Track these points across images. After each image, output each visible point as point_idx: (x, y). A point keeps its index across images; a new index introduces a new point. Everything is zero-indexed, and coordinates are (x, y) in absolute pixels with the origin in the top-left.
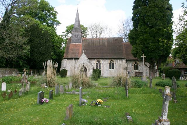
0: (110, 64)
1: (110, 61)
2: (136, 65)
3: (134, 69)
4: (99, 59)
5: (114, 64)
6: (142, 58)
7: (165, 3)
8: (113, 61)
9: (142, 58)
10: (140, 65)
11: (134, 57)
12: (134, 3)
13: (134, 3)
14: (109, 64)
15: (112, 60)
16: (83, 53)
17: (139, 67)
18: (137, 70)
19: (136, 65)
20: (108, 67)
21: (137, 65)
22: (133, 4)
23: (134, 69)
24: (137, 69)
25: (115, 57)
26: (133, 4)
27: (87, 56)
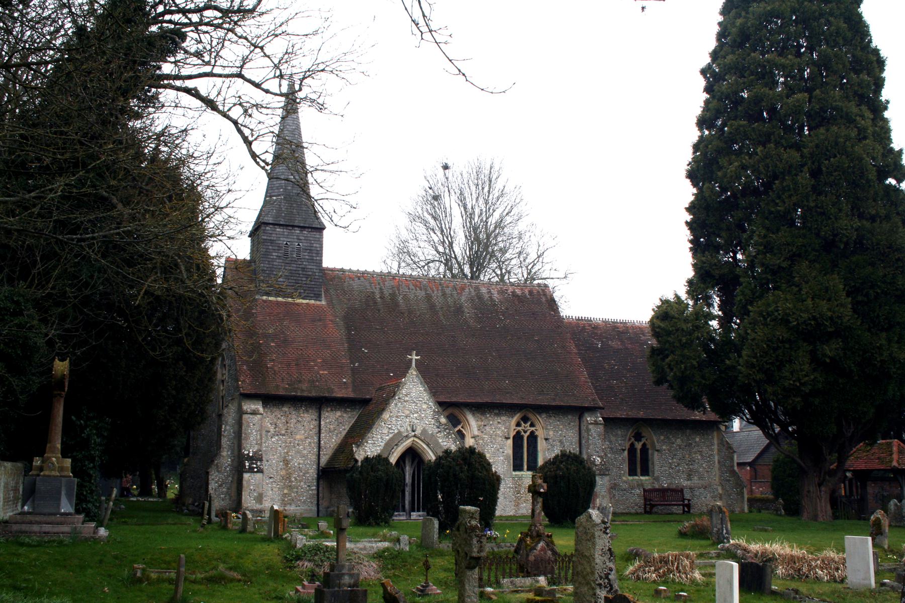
0: (518, 439)
1: (518, 425)
2: (638, 446)
3: (632, 472)
4: (456, 412)
5: (211, 577)
6: (412, 359)
7: (845, 109)
8: (532, 425)
9: (412, 359)
10: (658, 446)
11: (324, 228)
12: (689, 210)
13: (689, 210)
14: (510, 442)
15: (525, 419)
16: (413, 372)
17: (656, 460)
18: (642, 475)
19: (638, 446)
20: (507, 458)
21: (644, 449)
22: (720, 18)
23: (632, 472)
24: (645, 471)
25: (543, 400)
26: (706, 96)
27: (433, 391)
